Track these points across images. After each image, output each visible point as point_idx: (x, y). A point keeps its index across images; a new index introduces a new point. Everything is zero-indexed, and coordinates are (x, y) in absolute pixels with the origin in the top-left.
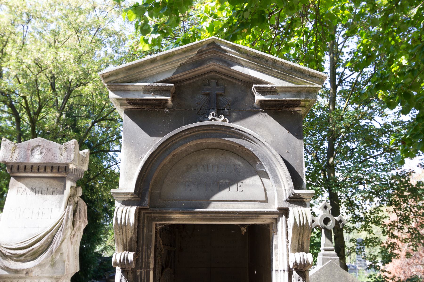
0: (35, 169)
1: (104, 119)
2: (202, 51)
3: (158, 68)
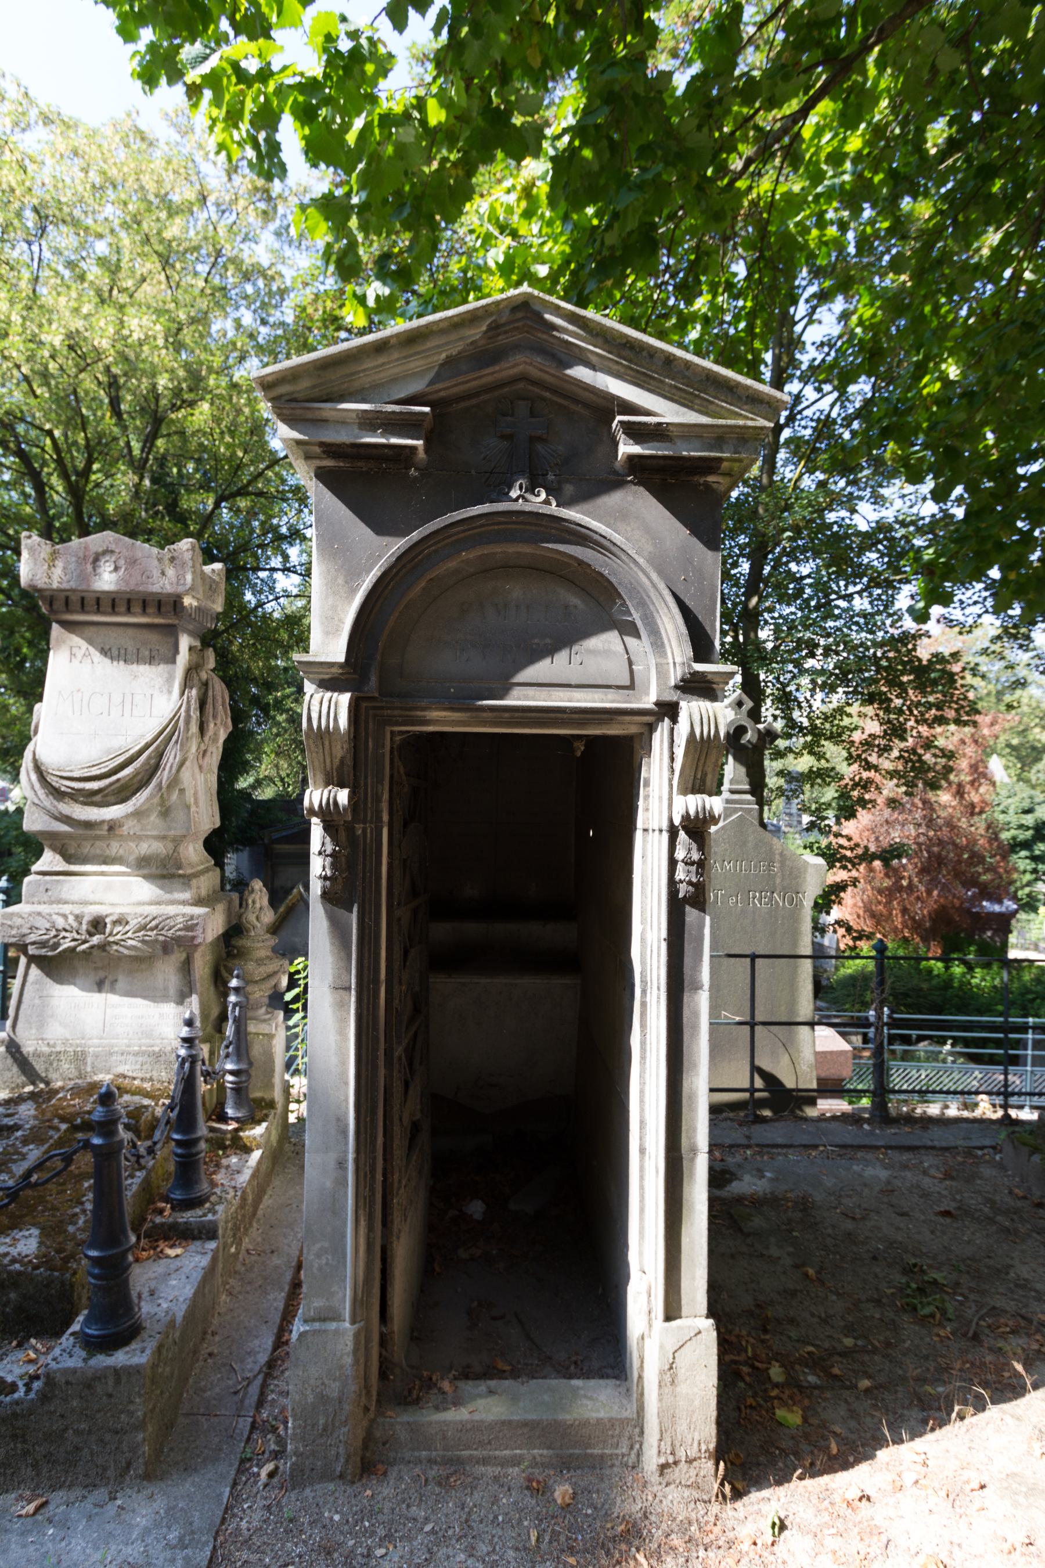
0: (106, 605)
1: (242, 492)
2: (498, 327)
3: (391, 366)
